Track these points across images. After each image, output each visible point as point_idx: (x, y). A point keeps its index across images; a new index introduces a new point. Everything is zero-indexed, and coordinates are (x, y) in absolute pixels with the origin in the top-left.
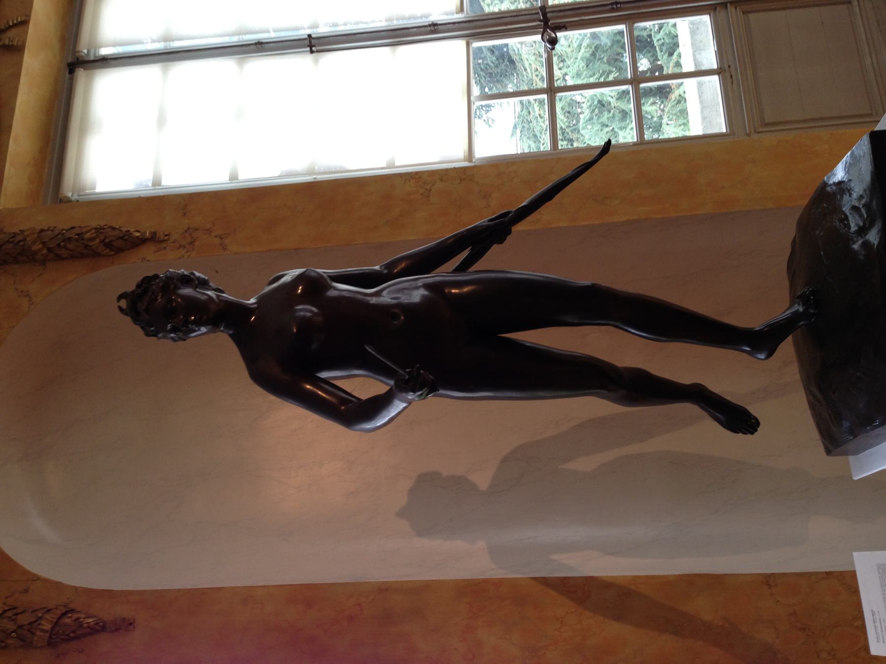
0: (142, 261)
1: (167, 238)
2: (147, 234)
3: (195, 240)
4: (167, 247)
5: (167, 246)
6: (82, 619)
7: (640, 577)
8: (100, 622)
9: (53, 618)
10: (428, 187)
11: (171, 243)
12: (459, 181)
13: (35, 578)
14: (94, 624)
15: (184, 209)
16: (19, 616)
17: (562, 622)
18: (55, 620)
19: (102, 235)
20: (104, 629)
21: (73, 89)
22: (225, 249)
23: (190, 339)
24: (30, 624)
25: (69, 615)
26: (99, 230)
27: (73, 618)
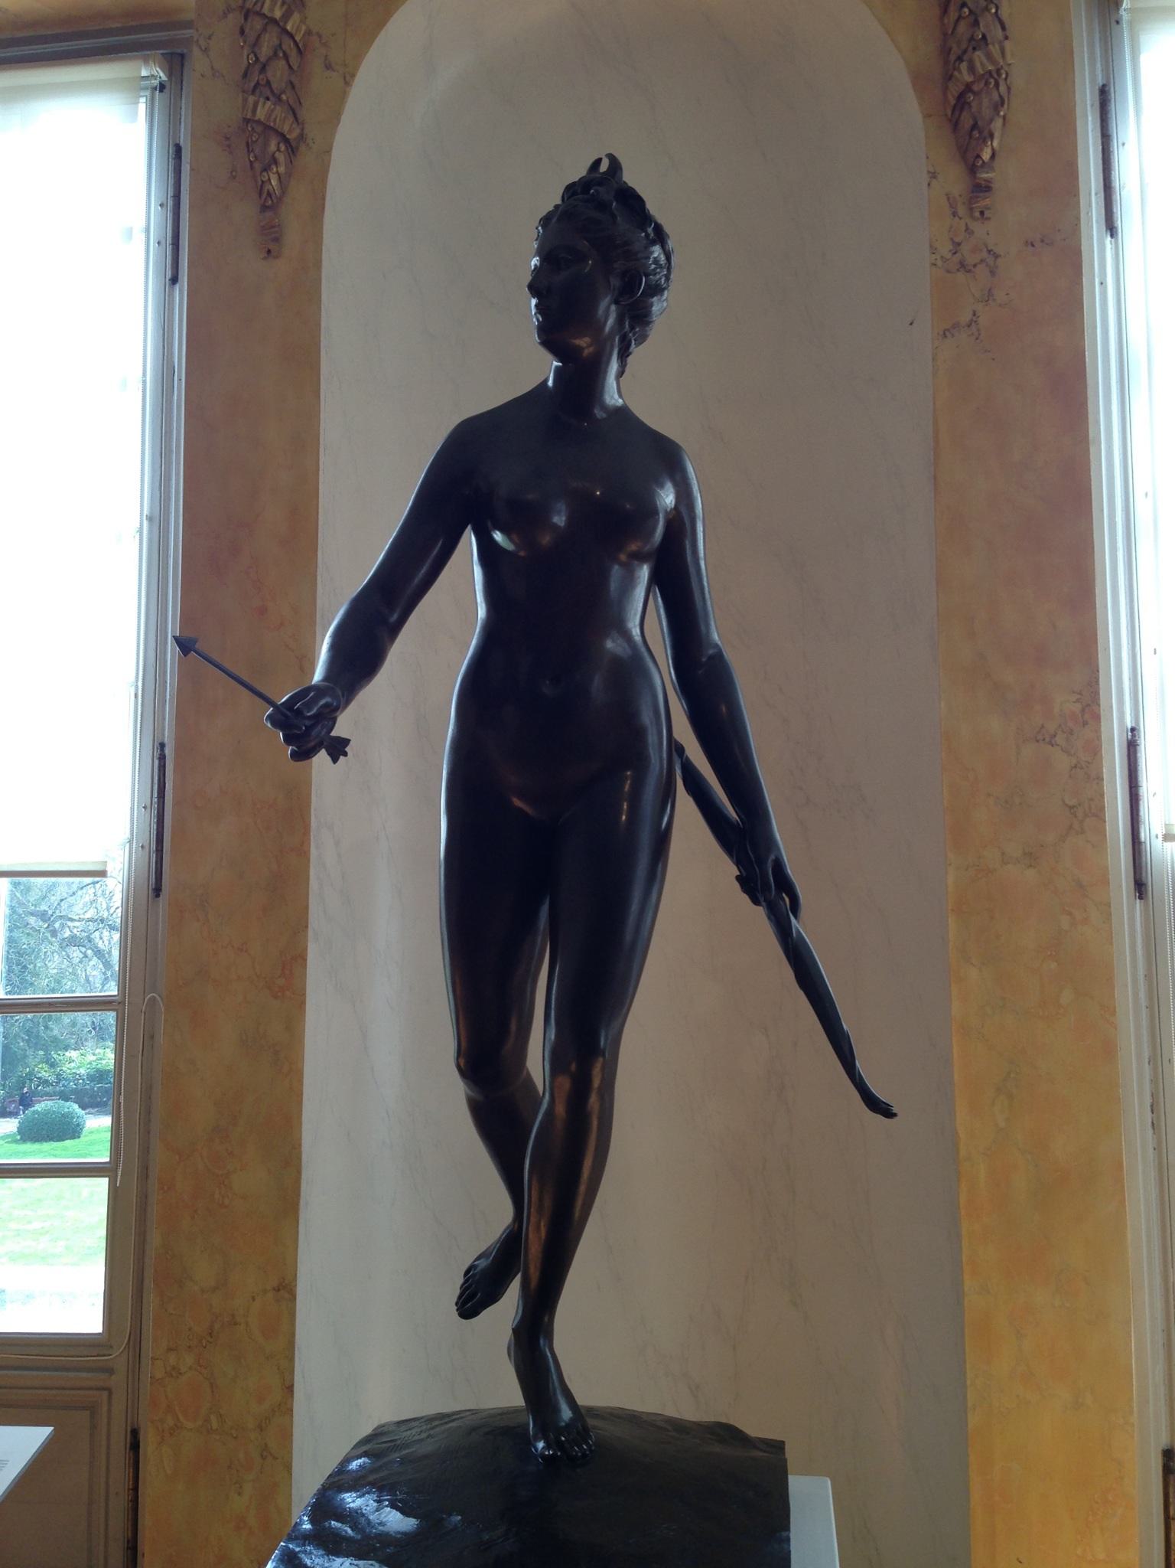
0: (929, 172)
1: (977, 214)
2: (985, 176)
3: (969, 271)
5: (960, 218)
6: (275, 169)
7: (300, 1081)
8: (272, 201)
9: (275, 119)
10: (1060, 739)
11: (966, 224)
12: (1071, 803)
13: (348, 79)
14: (268, 191)
15: (1042, 241)
16: (283, 62)
18: (272, 124)
19: (982, 84)
21: (32, 64)
22: (944, 334)
23: (627, 402)
24: (268, 83)
25: (283, 147)
26: (994, 76)
27: (277, 154)
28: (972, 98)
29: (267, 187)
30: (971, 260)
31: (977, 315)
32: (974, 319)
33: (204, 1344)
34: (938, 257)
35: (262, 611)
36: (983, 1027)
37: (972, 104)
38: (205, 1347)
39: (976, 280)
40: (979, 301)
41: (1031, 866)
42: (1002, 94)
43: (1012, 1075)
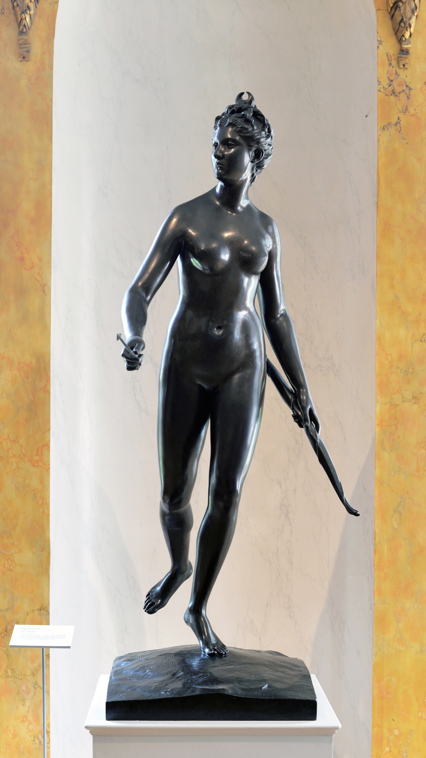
0: (378, 40)
2: (406, 46)
3: (397, 96)
4: (391, 67)
5: (393, 67)
7: (48, 509)
8: (26, 30)
11: (396, 70)
17: (15, 441)
20: (21, 33)
22: (384, 128)
28: (401, 5)
29: (24, 22)
30: (398, 89)
31: (400, 119)
32: (399, 121)
33: (3, 636)
34: (382, 87)
35: (22, 259)
36: (389, 481)
37: (401, 8)
38: (3, 637)
39: (400, 101)
40: (401, 112)
41: (415, 403)
42: (416, 4)
43: (402, 504)
